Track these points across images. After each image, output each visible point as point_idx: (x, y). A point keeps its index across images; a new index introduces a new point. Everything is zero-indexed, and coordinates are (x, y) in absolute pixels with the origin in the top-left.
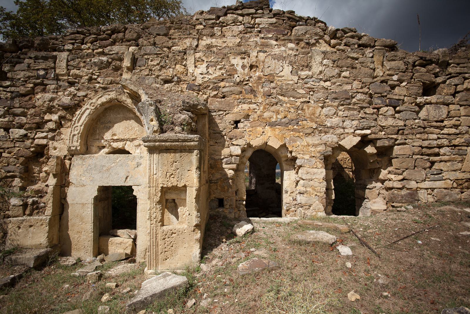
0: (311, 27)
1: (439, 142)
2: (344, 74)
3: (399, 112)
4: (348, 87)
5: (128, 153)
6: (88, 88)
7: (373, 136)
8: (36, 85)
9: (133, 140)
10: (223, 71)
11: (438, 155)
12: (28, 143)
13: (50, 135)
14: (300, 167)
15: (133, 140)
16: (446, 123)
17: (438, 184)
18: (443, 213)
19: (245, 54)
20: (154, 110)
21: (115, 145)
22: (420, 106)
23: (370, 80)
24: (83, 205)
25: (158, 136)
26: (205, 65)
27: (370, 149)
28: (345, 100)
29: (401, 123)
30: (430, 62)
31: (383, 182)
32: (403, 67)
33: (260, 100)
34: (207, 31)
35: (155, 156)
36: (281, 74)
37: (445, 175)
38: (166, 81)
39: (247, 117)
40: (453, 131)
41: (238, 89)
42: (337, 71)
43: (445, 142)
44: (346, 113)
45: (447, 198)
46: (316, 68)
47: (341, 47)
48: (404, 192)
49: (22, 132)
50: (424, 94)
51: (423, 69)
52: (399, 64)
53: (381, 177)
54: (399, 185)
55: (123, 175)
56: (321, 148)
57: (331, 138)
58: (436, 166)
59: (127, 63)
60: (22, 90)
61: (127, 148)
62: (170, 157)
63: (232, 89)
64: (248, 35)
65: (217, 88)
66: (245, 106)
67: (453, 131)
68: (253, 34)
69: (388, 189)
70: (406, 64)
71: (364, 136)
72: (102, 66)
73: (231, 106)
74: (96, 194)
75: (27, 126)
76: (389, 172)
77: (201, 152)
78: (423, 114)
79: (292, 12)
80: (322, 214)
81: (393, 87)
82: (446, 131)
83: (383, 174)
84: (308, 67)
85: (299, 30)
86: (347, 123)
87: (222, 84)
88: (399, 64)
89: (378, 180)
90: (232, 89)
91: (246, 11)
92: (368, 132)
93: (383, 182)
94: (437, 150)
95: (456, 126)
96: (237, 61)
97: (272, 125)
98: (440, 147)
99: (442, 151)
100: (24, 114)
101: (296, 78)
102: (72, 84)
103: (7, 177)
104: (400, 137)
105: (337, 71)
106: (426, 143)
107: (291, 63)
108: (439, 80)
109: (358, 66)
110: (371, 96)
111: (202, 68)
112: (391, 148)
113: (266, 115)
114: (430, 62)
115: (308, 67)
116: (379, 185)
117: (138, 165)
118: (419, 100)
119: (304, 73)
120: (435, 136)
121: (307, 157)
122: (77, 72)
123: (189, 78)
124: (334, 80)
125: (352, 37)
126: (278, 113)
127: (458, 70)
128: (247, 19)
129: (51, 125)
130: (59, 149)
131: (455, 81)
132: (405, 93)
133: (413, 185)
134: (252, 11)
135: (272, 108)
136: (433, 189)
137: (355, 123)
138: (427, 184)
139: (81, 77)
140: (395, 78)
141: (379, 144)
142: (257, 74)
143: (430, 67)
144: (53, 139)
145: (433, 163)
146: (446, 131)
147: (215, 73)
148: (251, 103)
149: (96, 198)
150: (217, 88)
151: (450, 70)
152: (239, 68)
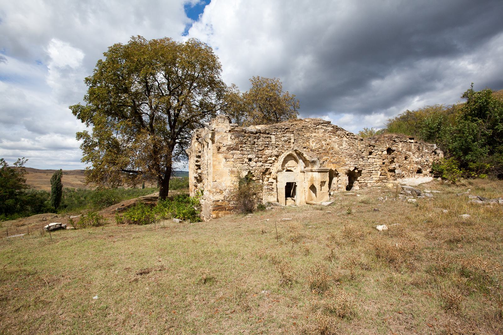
0: (342, 132)
1: (373, 169)
2: (351, 148)
3: (363, 160)
4: (352, 152)
5: (292, 171)
6: (282, 149)
7: (357, 167)
8: (265, 147)
9: (293, 167)
10: (320, 145)
11: (372, 173)
12: (263, 167)
13: (270, 165)
14: (339, 176)
15: (293, 167)
16: (374, 164)
17: (372, 181)
18: (374, 189)
19: (325, 140)
20: (112, 117)
21: (289, 169)
22: (368, 158)
23: (357, 150)
24: (282, 188)
25: (320, 168)
26: (315, 143)
27: (356, 171)
28: (351, 156)
29: (364, 163)
30: (371, 146)
31: (358, 181)
32: (365, 147)
33: (330, 155)
34: (314, 131)
35: (319, 173)
36: (335, 147)
37: (374, 179)
38: (305, 148)
39: (326, 160)
40: (375, 166)
41: (324, 151)
42: (349, 147)
43: (374, 169)
44: (352, 160)
45: (374, 185)
46: (344, 146)
47: (350, 139)
48: (364, 184)
49: (261, 164)
50: (370, 155)
51: (369, 148)
52: (364, 146)
53: (358, 179)
54: (363, 182)
55: (293, 178)
56: (345, 171)
57: (347, 168)
58: (372, 176)
59: (292, 141)
60: (261, 149)
61: (292, 170)
62: (323, 173)
63: (323, 151)
64: (325, 133)
65: (318, 151)
66: (326, 157)
67: (375, 166)
68: (327, 133)
69: (360, 183)
70: (366, 145)
71: (355, 167)
72: (285, 141)
73: (322, 157)
74: (286, 185)
75: (263, 161)
76: (361, 178)
77: (329, 173)
78: (369, 161)
79: (337, 126)
80: (345, 190)
81: (362, 152)
82: (374, 166)
83: (359, 178)
84: (342, 145)
85: (339, 132)
86: (352, 163)
87: (320, 150)
88: (364, 146)
89: (357, 180)
90: (323, 151)
91: (325, 125)
92: (356, 166)
93: (358, 181)
94: (372, 172)
95: (376, 165)
96: (324, 142)
97: (333, 163)
98: (372, 171)
99: (373, 172)
100: (261, 157)
101: (339, 149)
102: (276, 147)
103: (257, 179)
104: (363, 167)
105: (349, 147)
106: (369, 170)
107: (338, 144)
108: (373, 151)
109: (354, 145)
110: (357, 155)
111: (314, 144)
112: (361, 171)
113: (331, 160)
114: (371, 146)
115: (342, 145)
116: (357, 182)
117: (298, 175)
118: (369, 157)
119: (341, 147)
120: (371, 168)
121: (341, 173)
122: (278, 143)
123: (311, 147)
124: (348, 150)
125: (352, 136)
126: (334, 159)
127: (377, 148)
128: (324, 127)
129: (271, 161)
130: (273, 170)
131: (376, 151)
132: (365, 154)
133: (366, 182)
134: (326, 125)
135: (333, 158)
136: (371, 183)
137: (353, 163)
138: (370, 181)
139: (279, 145)
140: (363, 150)
141: (359, 169)
142: (329, 147)
143: (371, 147)
144: (271, 166)
145: (371, 175)
146: (374, 166)
147: (318, 146)
148: (327, 156)
149: (286, 186)
150: (318, 151)
151: (375, 148)
152: (324, 145)
